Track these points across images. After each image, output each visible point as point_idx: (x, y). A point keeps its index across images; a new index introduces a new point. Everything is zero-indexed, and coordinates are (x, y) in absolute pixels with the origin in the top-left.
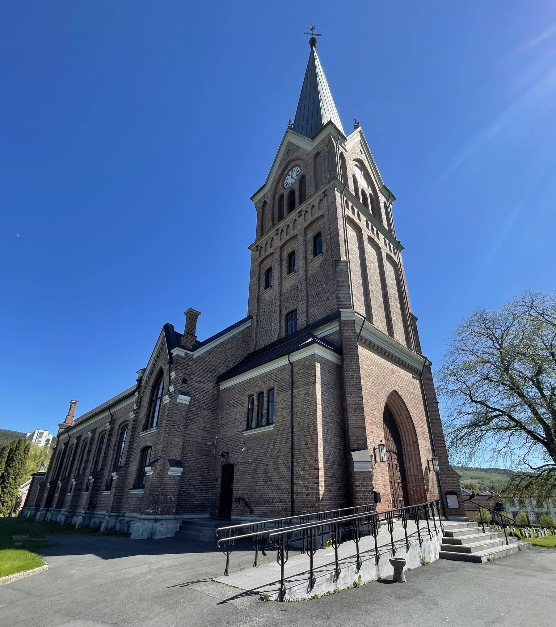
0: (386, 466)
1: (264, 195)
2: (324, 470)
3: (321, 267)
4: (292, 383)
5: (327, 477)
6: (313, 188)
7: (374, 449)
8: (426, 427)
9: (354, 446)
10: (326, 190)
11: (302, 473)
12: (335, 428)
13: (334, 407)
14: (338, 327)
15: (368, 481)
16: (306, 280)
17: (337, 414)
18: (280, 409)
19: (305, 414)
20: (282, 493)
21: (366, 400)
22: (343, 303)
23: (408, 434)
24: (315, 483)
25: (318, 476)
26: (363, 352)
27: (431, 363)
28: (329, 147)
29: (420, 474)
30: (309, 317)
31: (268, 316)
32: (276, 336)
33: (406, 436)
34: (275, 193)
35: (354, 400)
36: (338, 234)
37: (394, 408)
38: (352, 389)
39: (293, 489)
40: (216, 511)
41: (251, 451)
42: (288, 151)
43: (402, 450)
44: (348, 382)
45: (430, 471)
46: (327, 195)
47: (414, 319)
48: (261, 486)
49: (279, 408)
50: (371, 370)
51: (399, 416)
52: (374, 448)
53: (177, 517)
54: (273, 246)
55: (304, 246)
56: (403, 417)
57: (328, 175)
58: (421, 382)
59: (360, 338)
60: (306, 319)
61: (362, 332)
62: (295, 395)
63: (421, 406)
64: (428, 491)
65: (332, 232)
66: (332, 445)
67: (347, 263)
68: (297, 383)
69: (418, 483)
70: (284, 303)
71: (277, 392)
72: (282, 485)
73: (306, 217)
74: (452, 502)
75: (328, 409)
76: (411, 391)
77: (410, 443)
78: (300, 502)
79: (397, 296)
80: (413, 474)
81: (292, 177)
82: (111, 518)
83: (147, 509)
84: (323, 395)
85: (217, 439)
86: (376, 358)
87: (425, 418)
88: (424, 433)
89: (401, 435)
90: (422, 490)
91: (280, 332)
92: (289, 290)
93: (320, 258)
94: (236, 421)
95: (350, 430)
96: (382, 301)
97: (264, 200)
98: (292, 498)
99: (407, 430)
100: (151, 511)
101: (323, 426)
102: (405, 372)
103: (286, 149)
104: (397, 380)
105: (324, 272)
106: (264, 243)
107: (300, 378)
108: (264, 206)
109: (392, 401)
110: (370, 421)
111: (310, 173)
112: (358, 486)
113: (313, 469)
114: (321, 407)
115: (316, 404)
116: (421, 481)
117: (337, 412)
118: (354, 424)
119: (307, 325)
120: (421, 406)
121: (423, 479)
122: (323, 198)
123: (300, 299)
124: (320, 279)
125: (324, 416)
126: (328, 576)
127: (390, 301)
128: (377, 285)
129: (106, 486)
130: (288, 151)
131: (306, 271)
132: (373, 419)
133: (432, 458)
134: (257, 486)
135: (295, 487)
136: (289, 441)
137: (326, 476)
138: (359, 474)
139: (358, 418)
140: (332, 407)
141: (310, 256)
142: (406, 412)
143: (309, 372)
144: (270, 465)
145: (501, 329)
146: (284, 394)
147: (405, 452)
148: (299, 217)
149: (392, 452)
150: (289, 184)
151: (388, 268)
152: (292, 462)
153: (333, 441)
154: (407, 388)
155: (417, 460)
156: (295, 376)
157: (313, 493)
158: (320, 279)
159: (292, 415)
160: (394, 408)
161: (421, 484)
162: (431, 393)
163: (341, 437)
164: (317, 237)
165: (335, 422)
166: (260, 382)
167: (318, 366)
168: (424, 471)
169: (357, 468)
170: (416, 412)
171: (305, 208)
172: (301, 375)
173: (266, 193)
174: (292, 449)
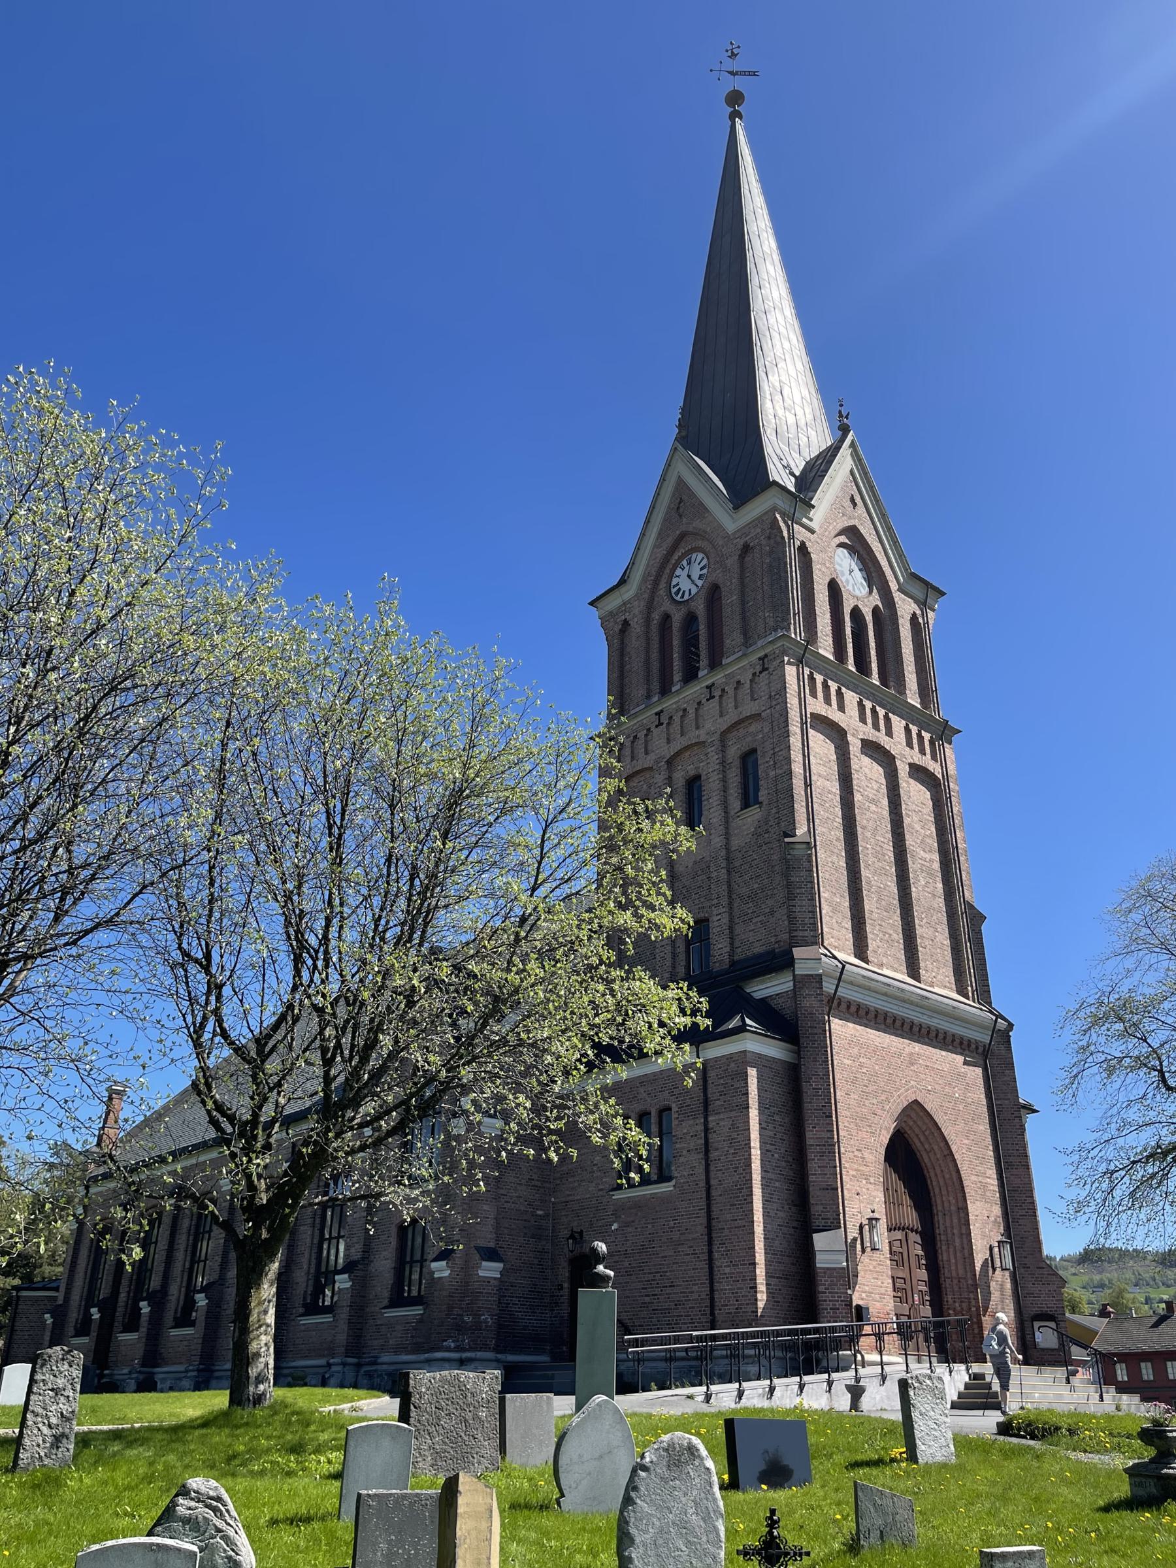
0: (886, 1258)
1: (624, 604)
2: (766, 1265)
4: (706, 1103)
5: (770, 1277)
6: (738, 638)
7: (861, 1227)
8: (992, 1173)
9: (818, 1222)
10: (766, 656)
11: (727, 1270)
13: (783, 1151)
14: (791, 984)
15: (841, 1285)
16: (727, 859)
18: (685, 1152)
20: (693, 1308)
22: (801, 933)
23: (948, 1191)
24: (751, 1288)
25: (755, 1276)
26: (841, 1030)
27: (1011, 1026)
28: (772, 541)
29: (969, 1275)
33: (942, 1196)
34: (650, 607)
36: (789, 773)
37: (917, 1135)
39: (712, 1299)
40: (564, 1348)
41: (630, 1229)
43: (933, 1223)
45: (994, 1270)
47: (977, 918)
48: (653, 1295)
49: (683, 1148)
50: (861, 1066)
51: (928, 1153)
52: (861, 1224)
53: (499, 1356)
55: (721, 776)
56: (935, 1154)
58: (985, 1070)
59: (835, 1002)
60: (728, 949)
61: (839, 989)
63: (984, 1127)
64: (985, 1311)
66: (780, 1221)
67: (810, 846)
68: (716, 1104)
69: (965, 1295)
71: (676, 1116)
72: (692, 1292)
73: (725, 704)
74: (1045, 1337)
76: (957, 1095)
77: (950, 1211)
78: (726, 1321)
79: (937, 866)
80: (954, 1274)
81: (689, 576)
82: (347, 1367)
83: (446, 1341)
84: (762, 1128)
85: (554, 1203)
86: (872, 1036)
87: (991, 1153)
88: (984, 1187)
89: (932, 1194)
90: (973, 1309)
93: (754, 815)
94: (595, 1168)
95: (812, 1194)
96: (896, 892)
97: (623, 618)
98: (712, 1314)
99: (946, 1183)
100: (453, 1345)
101: (764, 1186)
102: (944, 1053)
103: (673, 496)
104: (923, 1076)
108: (624, 632)
109: (911, 1123)
110: (854, 1173)
112: (823, 1293)
113: (745, 1264)
114: (759, 1152)
115: (750, 1148)
116: (972, 1289)
119: (733, 963)
121: (976, 1286)
125: (764, 1170)
126: (761, 1391)
127: (913, 889)
128: (884, 855)
129: (305, 1305)
130: (680, 503)
131: (727, 835)
133: (999, 1242)
134: (646, 1296)
135: (716, 1296)
136: (703, 1213)
137: (769, 1275)
138: (825, 1273)
139: (827, 1171)
141: (735, 804)
142: (942, 1144)
143: (737, 1085)
144: (670, 1256)
146: (691, 1122)
147: (940, 1229)
149: (908, 1228)
151: (916, 796)
152: (710, 1252)
153: (781, 1214)
154: (948, 1090)
155: (965, 1246)
156: (711, 1089)
157: (747, 1304)
159: (707, 1166)
160: (917, 1135)
161: (972, 1296)
162: (1009, 1096)
163: (795, 1205)
164: (749, 758)
166: (642, 1090)
167: (752, 1073)
168: (978, 1269)
169: (821, 1261)
170: (966, 1142)
172: (721, 1088)
173: (629, 602)
174: (709, 1227)
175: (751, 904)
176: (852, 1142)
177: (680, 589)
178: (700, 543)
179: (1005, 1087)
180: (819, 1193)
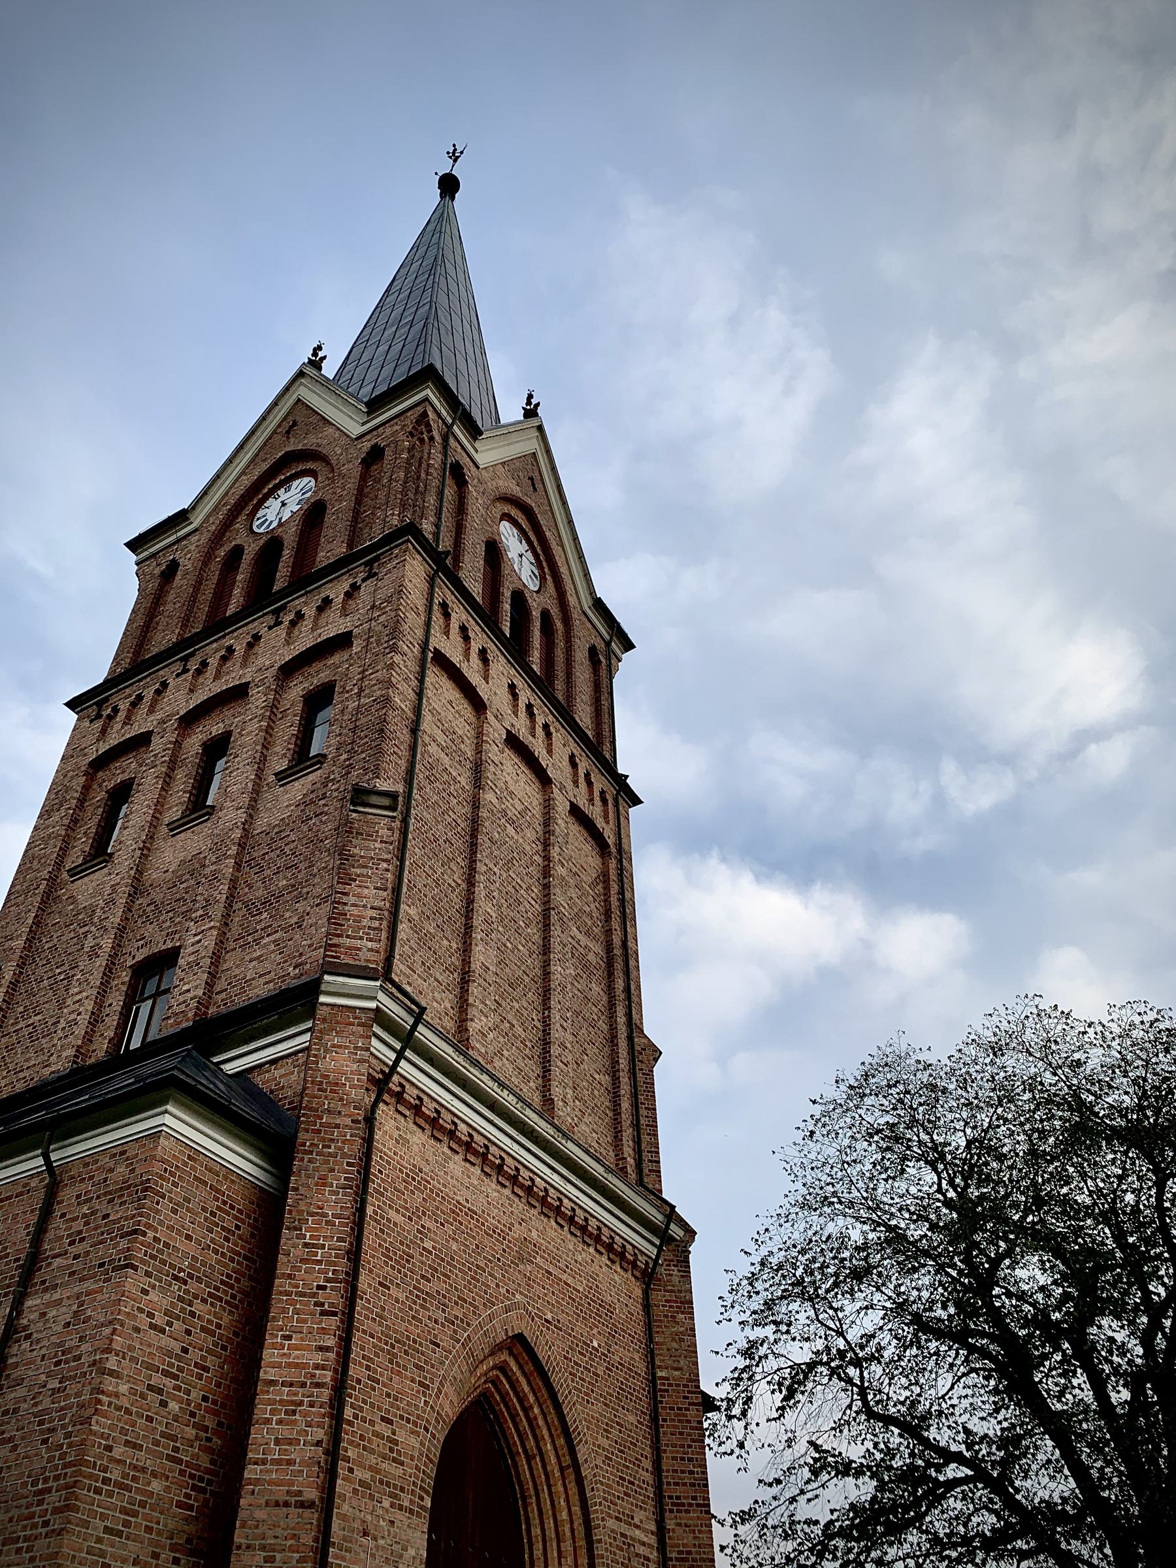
3: (305, 803)
12: (180, 1505)
13: (196, 1395)
16: (242, 845)
17: (205, 1429)
19: (41, 1423)
21: (368, 1368)
27: (691, 1233)
30: (217, 988)
31: (66, 967)
32: (70, 1052)
35: (297, 1366)
38: (296, 1312)
42: (290, 427)
44: (290, 1276)
46: (376, 574)
51: (529, 1459)
54: (158, 707)
57: (393, 514)
62: (25, 1322)
65: (367, 692)
70: (140, 921)
75: (164, 1404)
91: (89, 1037)
92: (169, 875)
95: (242, 1514)
97: (171, 557)
105: (311, 822)
106: (130, 696)
107: (72, 1243)
111: (340, 499)
117: (210, 1422)
118: (271, 1482)
120: (632, 1418)
122: (364, 580)
123: (201, 912)
124: (292, 846)
132: (384, 1466)
140: (188, 1393)
145: (964, 1131)
148: (270, 628)
150: (271, 522)
156: (58, 1227)
158: (292, 846)
165: (182, 1473)
171: (297, 602)
172: (78, 1225)
175: (265, 915)
176: (374, 1397)
177: (267, 520)
178: (310, 465)
179: (675, 1345)
180: (260, 1514)
